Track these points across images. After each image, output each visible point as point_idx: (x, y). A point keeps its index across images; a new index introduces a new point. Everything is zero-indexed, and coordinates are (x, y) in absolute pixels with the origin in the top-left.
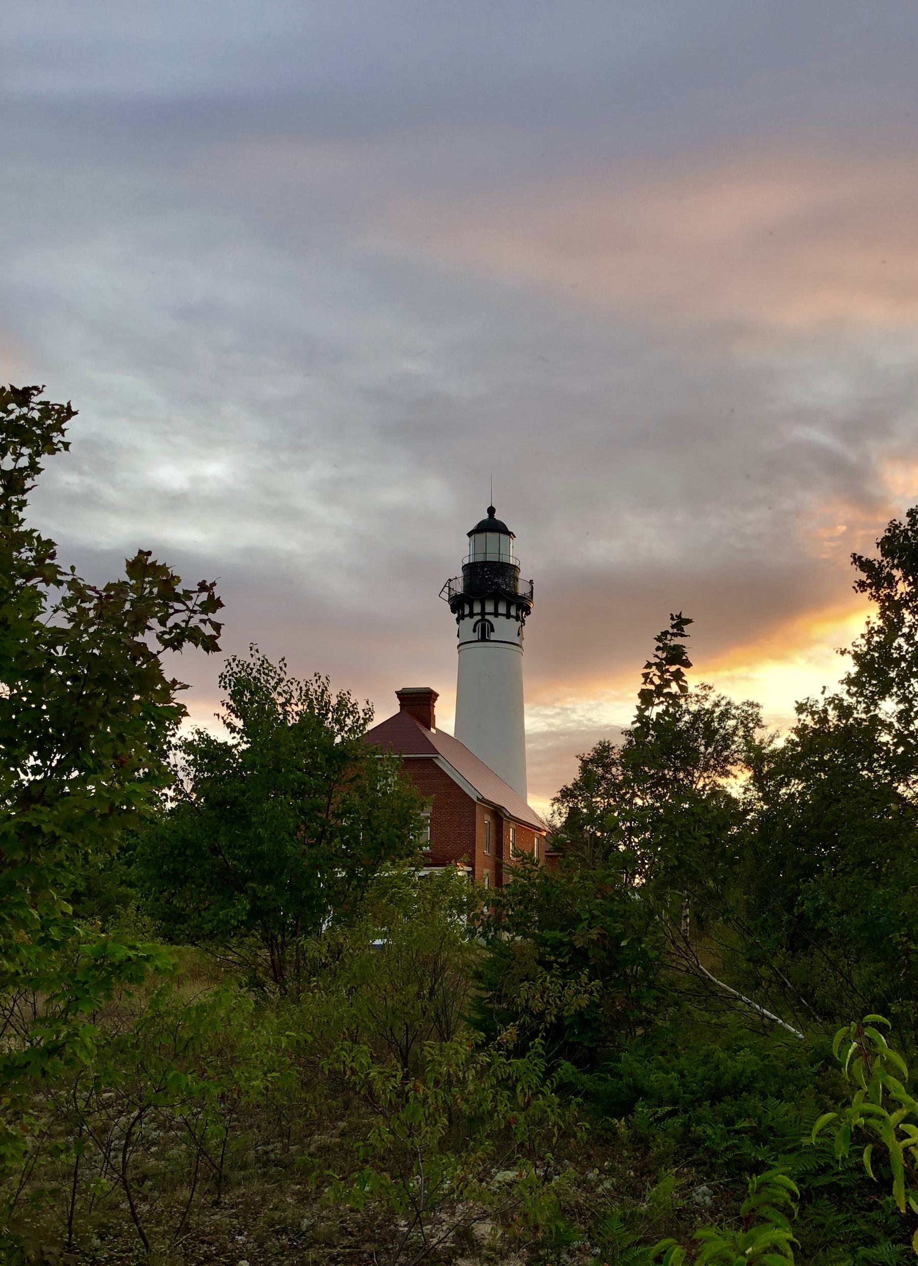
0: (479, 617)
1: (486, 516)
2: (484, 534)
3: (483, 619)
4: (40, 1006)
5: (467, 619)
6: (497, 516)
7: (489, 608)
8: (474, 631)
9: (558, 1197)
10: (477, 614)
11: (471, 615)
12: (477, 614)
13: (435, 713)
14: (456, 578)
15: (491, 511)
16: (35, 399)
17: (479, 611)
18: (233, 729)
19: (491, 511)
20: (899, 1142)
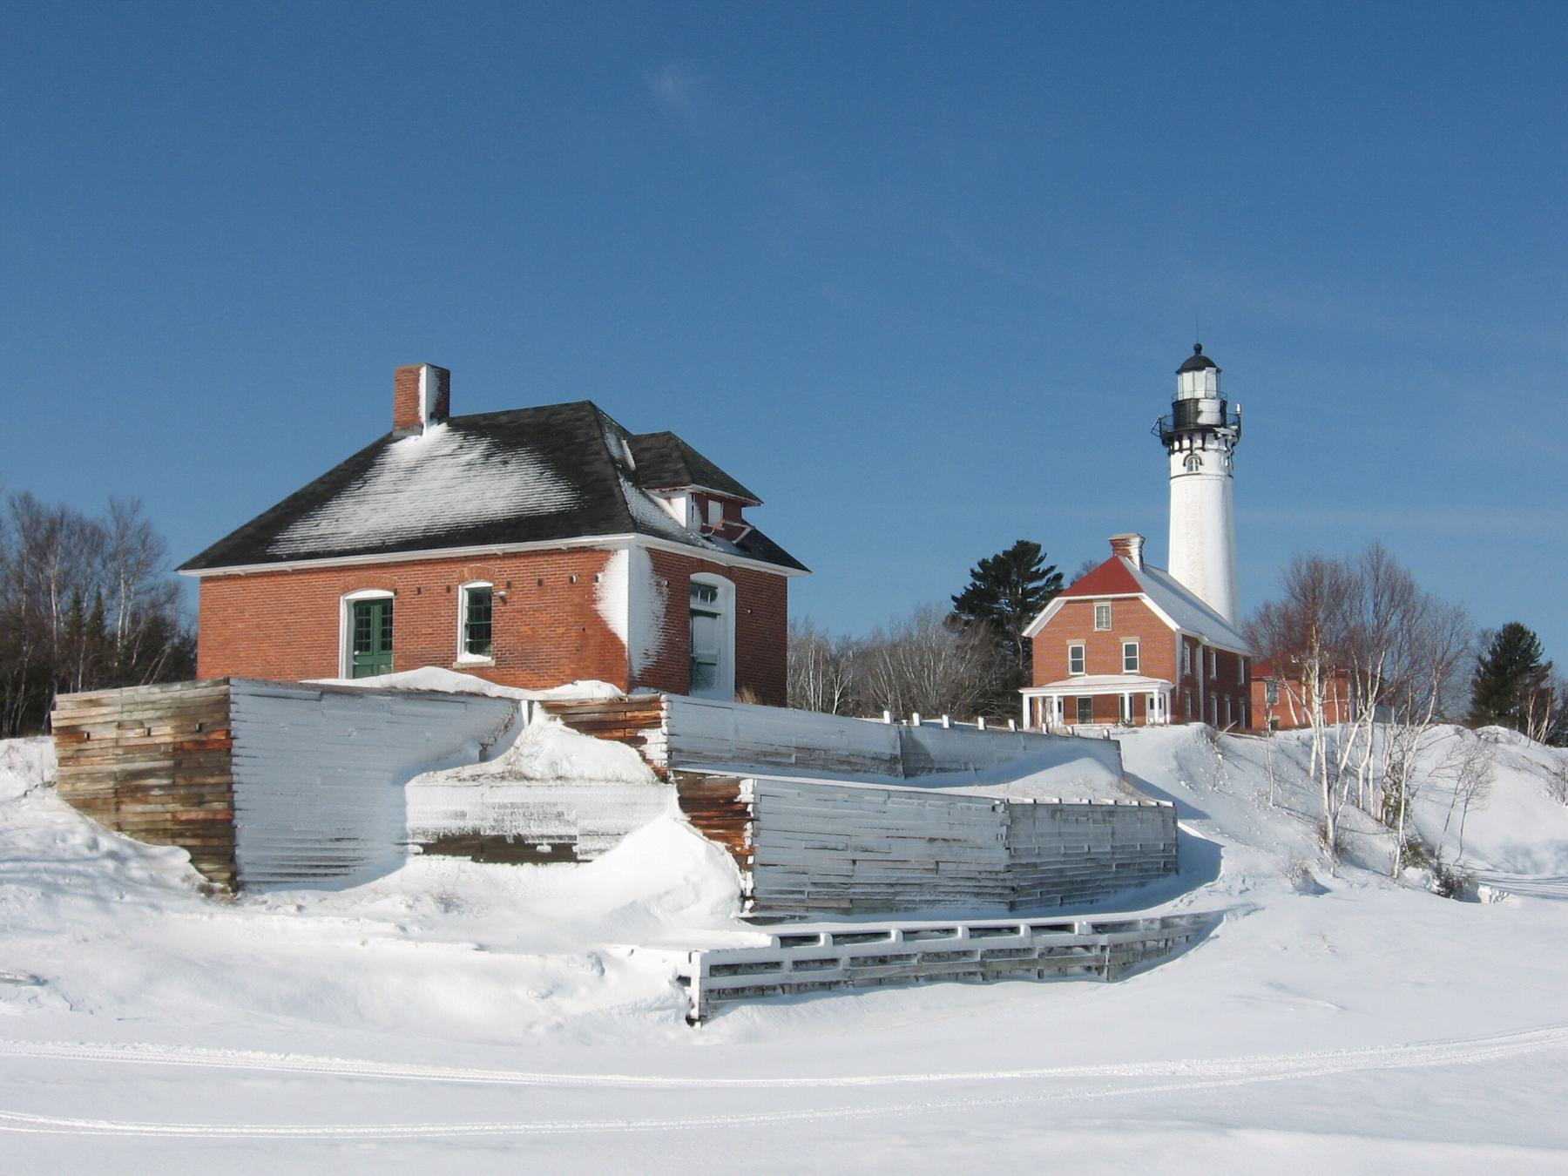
1: (1193, 353)
2: (1191, 373)
3: (1191, 454)
4: (488, 494)
5: (1177, 454)
6: (1204, 353)
7: (1198, 443)
8: (1184, 465)
9: (1011, 856)
10: (1186, 449)
11: (1181, 450)
12: (1186, 449)
13: (525, 864)
14: (1166, 417)
15: (1198, 349)
16: (1509, 736)
17: (1189, 446)
18: (1294, 578)
19: (1198, 349)
20: (1130, 694)
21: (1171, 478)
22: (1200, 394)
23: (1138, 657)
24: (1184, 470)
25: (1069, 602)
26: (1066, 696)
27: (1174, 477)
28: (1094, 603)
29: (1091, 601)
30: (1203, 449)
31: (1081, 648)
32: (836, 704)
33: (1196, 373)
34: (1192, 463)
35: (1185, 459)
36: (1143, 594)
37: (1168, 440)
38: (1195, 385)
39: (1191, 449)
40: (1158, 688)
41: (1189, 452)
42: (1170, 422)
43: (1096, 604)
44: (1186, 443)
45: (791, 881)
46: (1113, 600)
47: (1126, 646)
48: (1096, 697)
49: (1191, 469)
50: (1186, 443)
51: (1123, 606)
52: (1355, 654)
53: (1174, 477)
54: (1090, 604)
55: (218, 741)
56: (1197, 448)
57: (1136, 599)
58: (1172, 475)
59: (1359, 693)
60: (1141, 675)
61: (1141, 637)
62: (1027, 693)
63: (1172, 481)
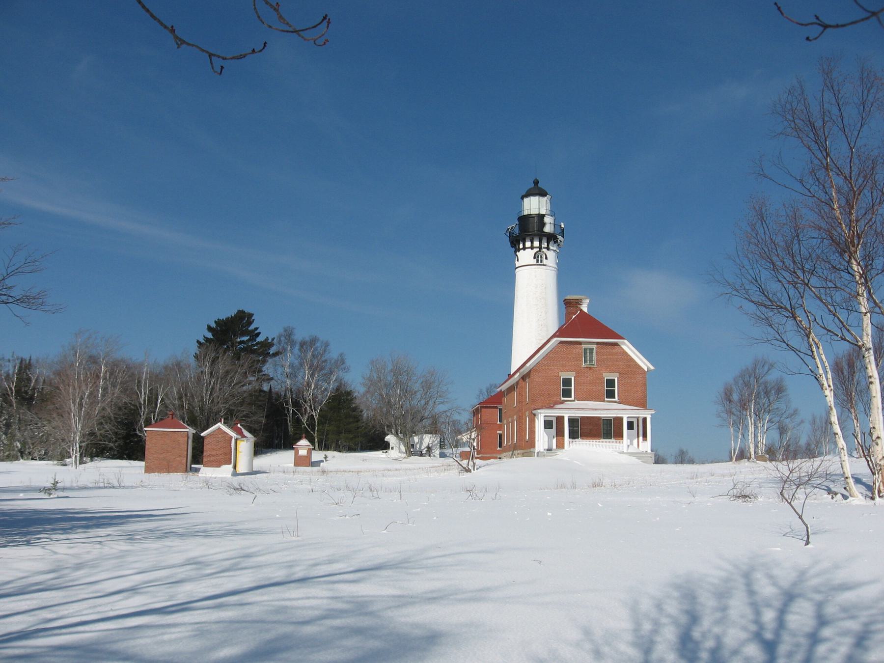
0: (538, 249)
7: (545, 245)
8: (534, 258)
11: (532, 248)
15: (536, 183)
19: (536, 183)
21: (517, 268)
22: (543, 212)
23: (562, 387)
24: (534, 261)
25: (562, 343)
26: (558, 416)
27: (518, 267)
28: (582, 345)
29: (580, 343)
30: (548, 249)
31: (614, 380)
32: (159, 405)
33: (540, 198)
34: (538, 258)
35: (535, 254)
36: (626, 341)
37: (516, 242)
38: (534, 205)
39: (540, 248)
40: (651, 415)
41: (538, 249)
42: (517, 231)
43: (584, 346)
44: (536, 244)
45: (89, 534)
46: (598, 344)
47: (607, 379)
48: (582, 418)
49: (537, 261)
50: (536, 244)
51: (607, 349)
52: (592, 389)
53: (518, 267)
54: (578, 346)
55: (550, 513)
56: (544, 248)
57: (616, 344)
58: (517, 266)
59: (14, 395)
60: (620, 403)
61: (620, 374)
62: (543, 413)
63: (517, 270)
